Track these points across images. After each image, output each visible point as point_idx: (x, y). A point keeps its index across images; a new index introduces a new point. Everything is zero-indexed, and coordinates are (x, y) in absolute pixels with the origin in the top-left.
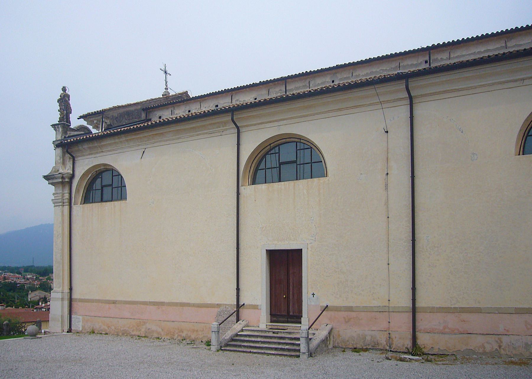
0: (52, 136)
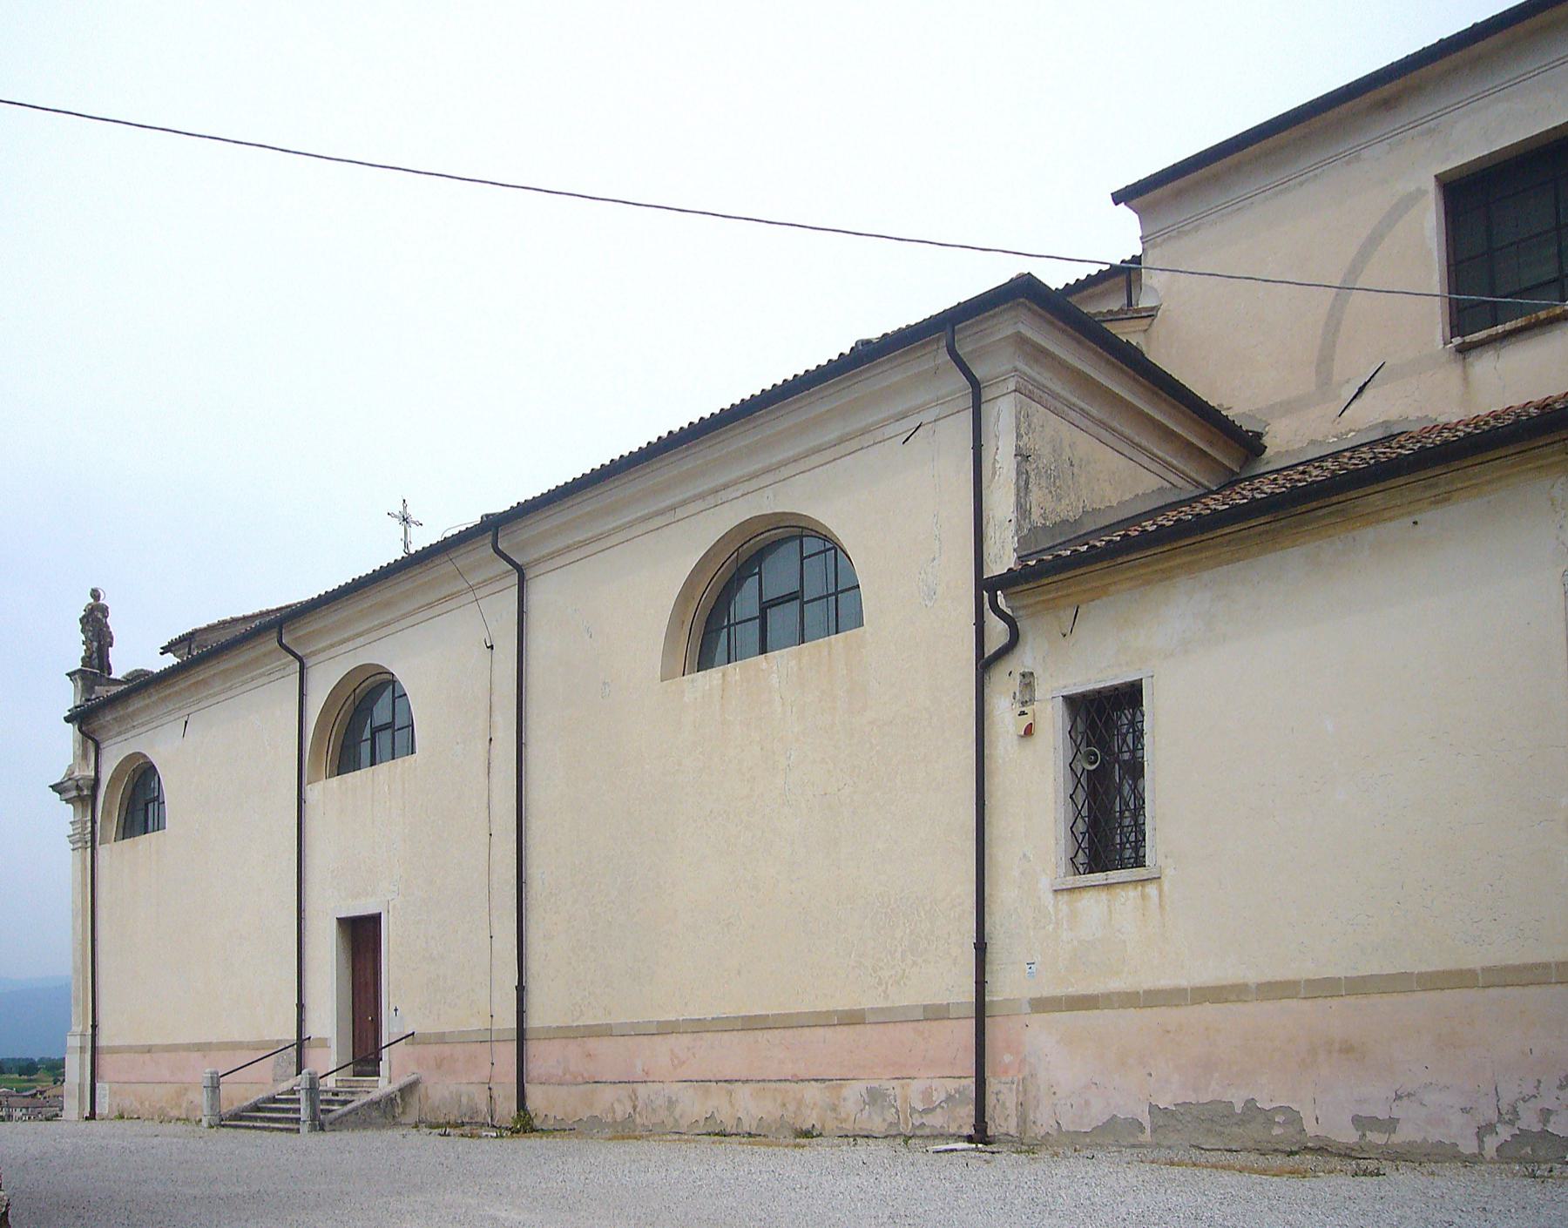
0: (68, 696)
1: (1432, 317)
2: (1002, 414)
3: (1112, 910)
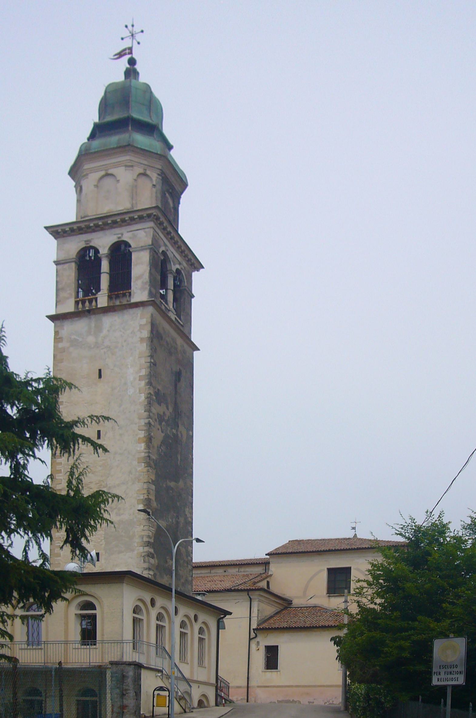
1: (325, 591)
2: (255, 604)
3: (271, 675)
